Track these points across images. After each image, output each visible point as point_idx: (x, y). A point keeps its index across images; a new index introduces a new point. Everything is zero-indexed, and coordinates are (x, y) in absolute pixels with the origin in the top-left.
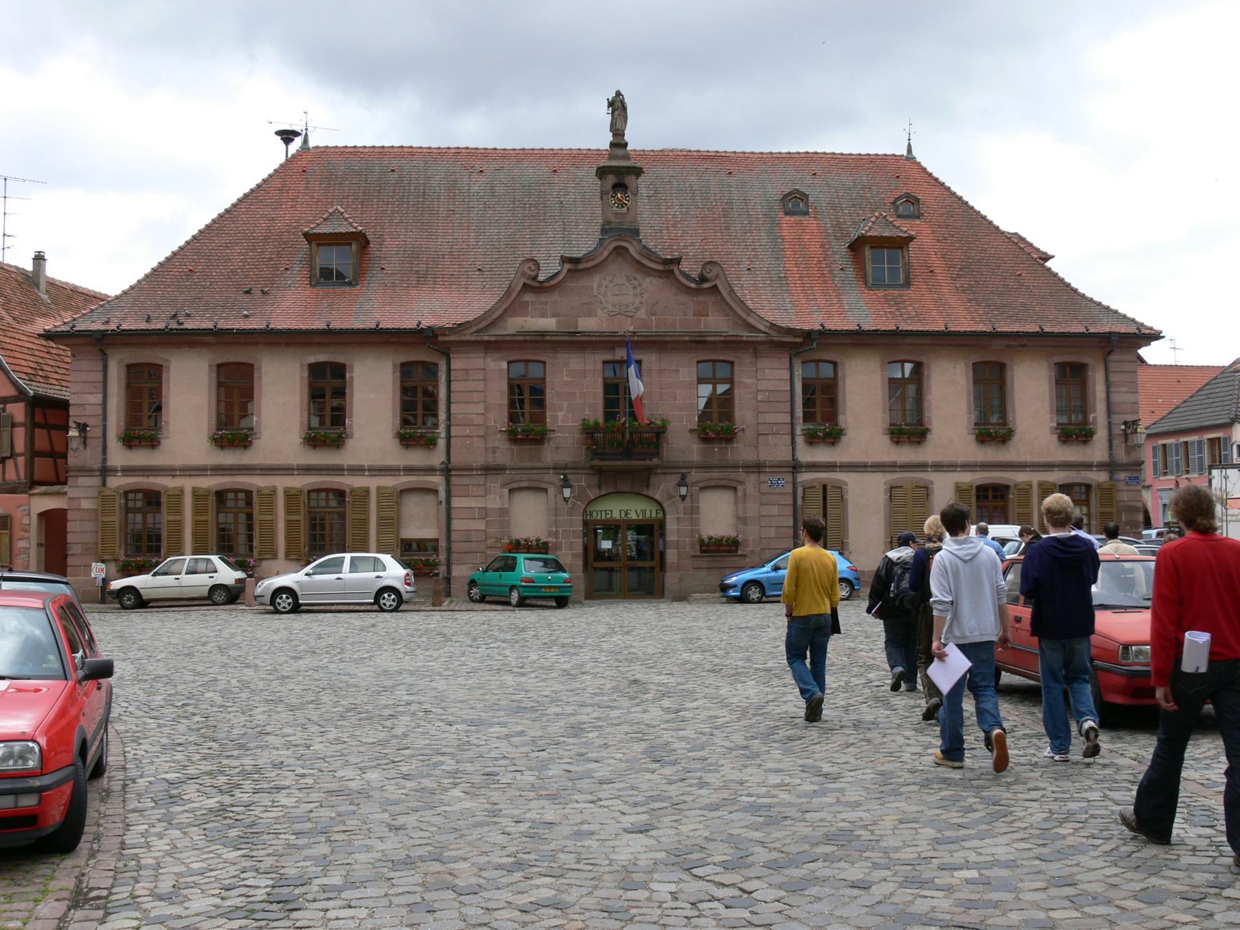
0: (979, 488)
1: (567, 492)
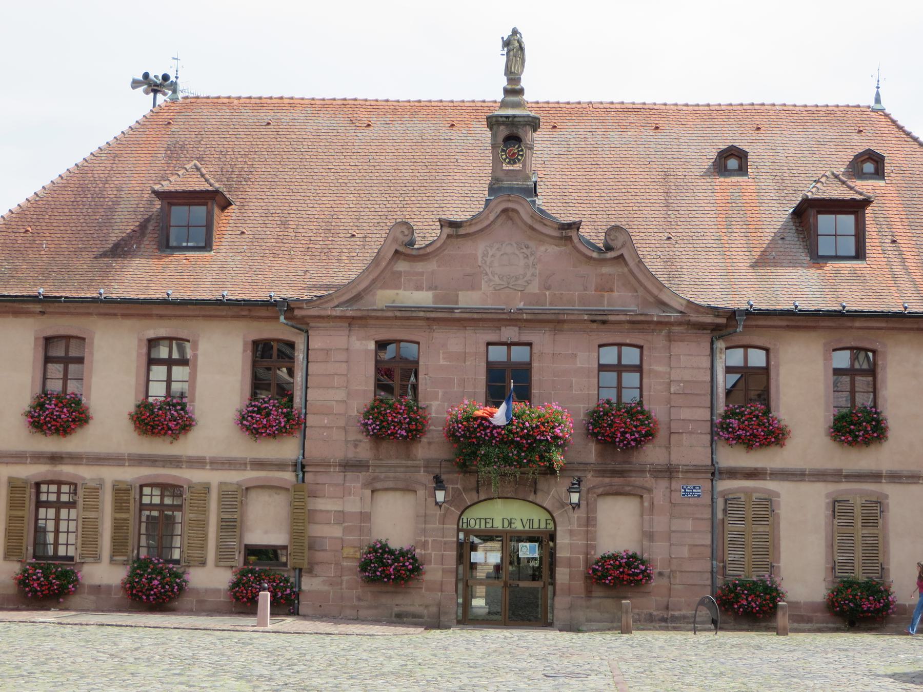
1: (440, 496)
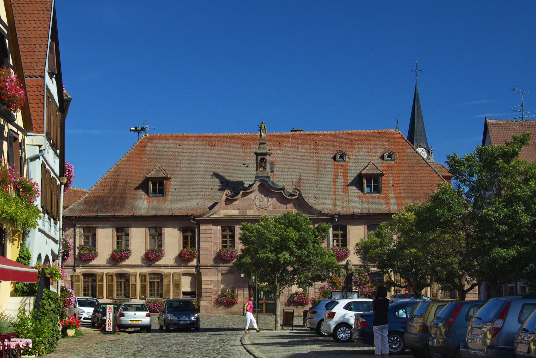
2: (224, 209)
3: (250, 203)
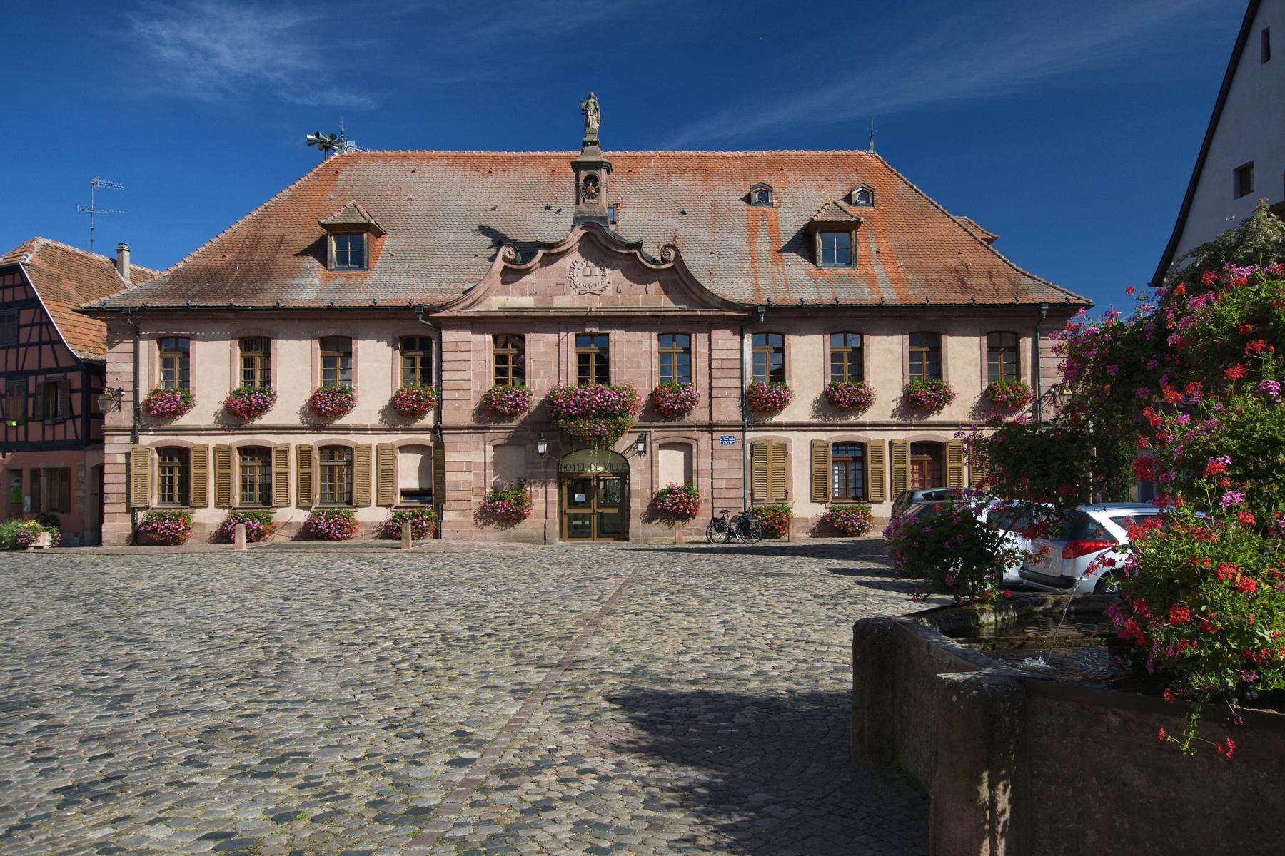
0: (913, 445)
2: (499, 293)
3: (560, 280)
